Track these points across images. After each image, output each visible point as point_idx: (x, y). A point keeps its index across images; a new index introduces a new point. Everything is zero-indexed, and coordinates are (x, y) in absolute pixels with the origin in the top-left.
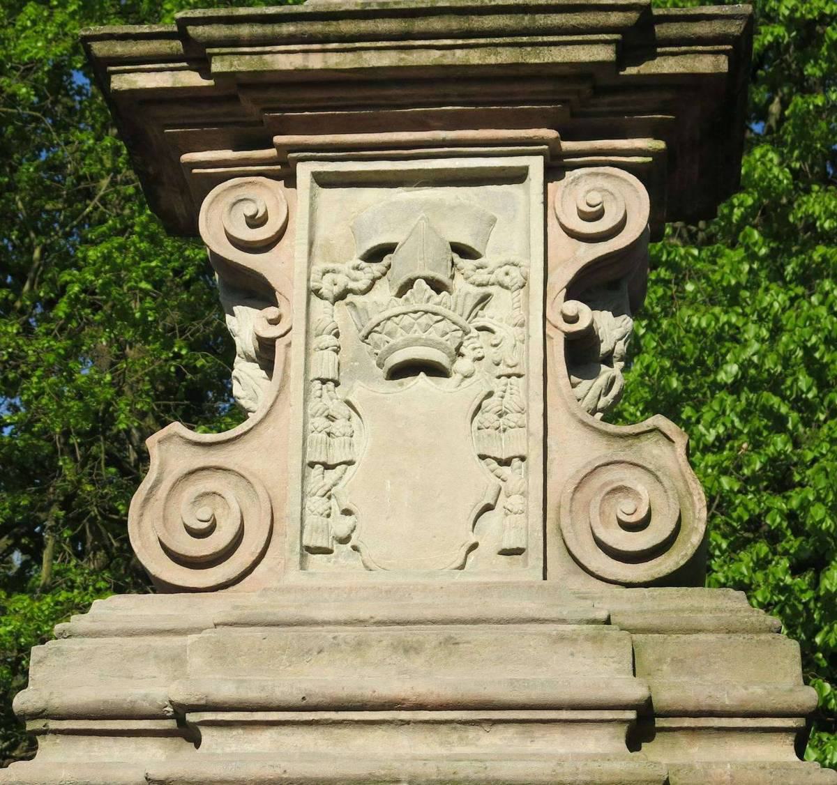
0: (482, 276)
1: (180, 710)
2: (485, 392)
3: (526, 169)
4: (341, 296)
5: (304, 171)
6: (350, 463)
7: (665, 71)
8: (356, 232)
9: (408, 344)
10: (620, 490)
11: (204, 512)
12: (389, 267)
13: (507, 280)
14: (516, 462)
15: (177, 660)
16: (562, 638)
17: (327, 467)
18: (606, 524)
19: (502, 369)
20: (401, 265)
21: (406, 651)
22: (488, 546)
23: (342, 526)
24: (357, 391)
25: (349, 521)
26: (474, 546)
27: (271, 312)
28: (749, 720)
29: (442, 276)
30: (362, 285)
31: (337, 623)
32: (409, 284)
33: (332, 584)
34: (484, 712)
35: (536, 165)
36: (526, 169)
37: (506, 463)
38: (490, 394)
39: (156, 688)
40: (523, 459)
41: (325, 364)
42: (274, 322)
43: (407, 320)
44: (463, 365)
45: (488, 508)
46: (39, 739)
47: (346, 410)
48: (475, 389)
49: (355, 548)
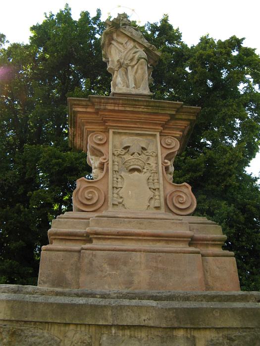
0: (147, 154)
1: (88, 234)
2: (115, 207)
3: (156, 135)
4: (118, 155)
5: (111, 131)
6: (122, 188)
7: (31, 286)
8: (121, 144)
9: (135, 165)
10: (180, 196)
11: (90, 195)
12: (128, 151)
13: (153, 155)
14: (157, 190)
15: (88, 225)
16: (174, 222)
17: (117, 188)
18: (176, 203)
19: (152, 172)
20: (131, 150)
21: (140, 224)
22: (152, 206)
23: (121, 200)
24: (123, 174)
25: (122, 199)
26: (149, 206)
27: (103, 157)
28: (213, 242)
29: (140, 153)
30: (123, 153)
31: (123, 218)
32: (134, 153)
33: (120, 212)
34: (157, 238)
35: (158, 134)
36: (156, 135)
37: (155, 190)
38: (151, 176)
39: (80, 229)
40: (158, 189)
41: (116, 168)
42: (105, 159)
43: (133, 160)
44: (145, 170)
45: (152, 198)
46: (53, 241)
47: (120, 177)
48: (148, 175)
49: (123, 205)
